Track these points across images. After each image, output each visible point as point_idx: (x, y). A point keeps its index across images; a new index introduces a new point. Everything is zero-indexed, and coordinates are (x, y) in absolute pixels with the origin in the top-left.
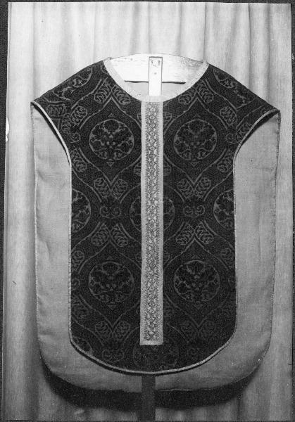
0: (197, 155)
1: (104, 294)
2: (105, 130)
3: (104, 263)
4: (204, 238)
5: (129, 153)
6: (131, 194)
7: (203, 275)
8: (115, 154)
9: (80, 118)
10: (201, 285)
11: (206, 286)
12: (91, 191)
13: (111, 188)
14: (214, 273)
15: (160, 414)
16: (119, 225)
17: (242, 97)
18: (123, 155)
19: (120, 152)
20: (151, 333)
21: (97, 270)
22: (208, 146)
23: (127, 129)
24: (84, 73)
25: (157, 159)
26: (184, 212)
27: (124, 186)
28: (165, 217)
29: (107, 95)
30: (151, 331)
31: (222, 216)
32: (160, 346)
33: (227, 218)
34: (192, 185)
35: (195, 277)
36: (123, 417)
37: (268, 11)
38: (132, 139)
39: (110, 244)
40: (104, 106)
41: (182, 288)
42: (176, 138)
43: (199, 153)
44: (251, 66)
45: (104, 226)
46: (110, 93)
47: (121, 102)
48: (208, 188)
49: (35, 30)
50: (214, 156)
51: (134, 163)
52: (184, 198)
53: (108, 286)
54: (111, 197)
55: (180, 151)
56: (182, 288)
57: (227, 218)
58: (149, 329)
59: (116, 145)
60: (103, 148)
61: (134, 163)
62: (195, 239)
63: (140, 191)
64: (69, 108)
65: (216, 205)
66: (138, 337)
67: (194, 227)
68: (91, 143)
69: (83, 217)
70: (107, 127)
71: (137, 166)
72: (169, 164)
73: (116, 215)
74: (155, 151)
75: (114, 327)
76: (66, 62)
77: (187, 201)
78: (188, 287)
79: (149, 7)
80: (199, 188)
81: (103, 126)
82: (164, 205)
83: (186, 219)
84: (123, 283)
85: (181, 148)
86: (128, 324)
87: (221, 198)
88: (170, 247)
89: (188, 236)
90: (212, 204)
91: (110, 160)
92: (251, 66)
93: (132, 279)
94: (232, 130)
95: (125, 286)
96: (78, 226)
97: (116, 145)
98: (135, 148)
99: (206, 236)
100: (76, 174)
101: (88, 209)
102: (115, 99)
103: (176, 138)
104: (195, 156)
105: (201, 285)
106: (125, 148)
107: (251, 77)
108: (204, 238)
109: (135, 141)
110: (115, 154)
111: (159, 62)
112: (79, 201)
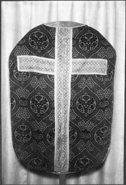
1: (36, 45)
2: (36, 99)
9: (24, 157)
13: (86, 125)
15: (72, 181)
16: (42, 78)
19: (92, 47)
22: (92, 107)
29: (37, 84)
34: (87, 85)
35: (88, 40)
36: (46, 181)
37: (115, 5)
39: (38, 150)
41: (80, 107)
44: (107, 23)
45: (35, 78)
46: (38, 83)
52: (100, 99)
54: (85, 129)
56: (80, 107)
59: (41, 43)
70: (36, 35)
73: (40, 138)
76: (26, 4)
77: (83, 131)
78: (82, 106)
84: (44, 105)
91: (38, 114)
92: (107, 23)
97: (41, 43)
108: (90, 85)
109: (49, 42)
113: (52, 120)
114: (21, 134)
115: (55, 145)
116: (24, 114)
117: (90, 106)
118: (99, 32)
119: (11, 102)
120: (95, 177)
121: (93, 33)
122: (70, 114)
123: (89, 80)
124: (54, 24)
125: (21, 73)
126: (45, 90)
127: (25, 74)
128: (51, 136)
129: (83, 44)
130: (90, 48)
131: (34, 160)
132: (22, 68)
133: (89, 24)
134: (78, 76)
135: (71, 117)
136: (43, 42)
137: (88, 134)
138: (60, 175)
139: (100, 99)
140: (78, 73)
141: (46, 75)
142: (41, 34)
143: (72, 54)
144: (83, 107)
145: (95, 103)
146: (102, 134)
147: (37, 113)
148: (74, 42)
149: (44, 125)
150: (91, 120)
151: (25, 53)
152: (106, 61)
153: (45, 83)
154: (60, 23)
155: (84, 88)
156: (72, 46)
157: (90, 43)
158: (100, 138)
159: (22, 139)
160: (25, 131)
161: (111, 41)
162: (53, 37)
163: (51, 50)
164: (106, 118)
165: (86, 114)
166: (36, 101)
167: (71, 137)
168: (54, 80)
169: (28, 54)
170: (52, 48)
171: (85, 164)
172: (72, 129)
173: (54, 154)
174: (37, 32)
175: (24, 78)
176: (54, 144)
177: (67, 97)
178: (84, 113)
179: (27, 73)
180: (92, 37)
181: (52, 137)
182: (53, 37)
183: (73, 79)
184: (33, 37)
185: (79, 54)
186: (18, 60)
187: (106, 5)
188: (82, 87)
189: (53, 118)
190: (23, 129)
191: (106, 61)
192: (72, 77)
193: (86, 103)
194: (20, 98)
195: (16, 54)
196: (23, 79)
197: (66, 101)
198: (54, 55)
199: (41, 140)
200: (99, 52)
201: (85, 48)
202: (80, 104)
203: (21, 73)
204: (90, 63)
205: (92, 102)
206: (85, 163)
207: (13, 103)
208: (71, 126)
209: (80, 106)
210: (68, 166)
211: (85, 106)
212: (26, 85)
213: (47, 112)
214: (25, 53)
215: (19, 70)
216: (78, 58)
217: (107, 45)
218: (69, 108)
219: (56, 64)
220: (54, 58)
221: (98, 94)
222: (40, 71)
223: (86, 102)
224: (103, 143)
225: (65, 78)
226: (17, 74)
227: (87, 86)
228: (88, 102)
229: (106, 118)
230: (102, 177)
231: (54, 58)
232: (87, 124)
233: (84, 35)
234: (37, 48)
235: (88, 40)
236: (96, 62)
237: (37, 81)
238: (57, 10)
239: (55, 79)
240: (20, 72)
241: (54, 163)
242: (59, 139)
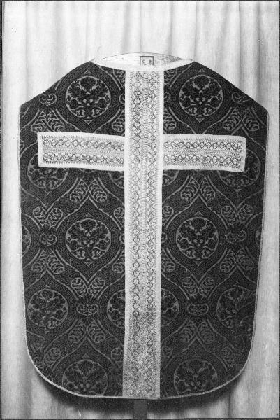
8: (93, 111)
10: (202, 241)
11: (207, 243)
21: (76, 227)
23: (103, 86)
27: (211, 283)
35: (197, 234)
49: (27, 37)
52: (227, 225)
53: (85, 242)
54: (198, 295)
59: (94, 102)
60: (190, 247)
68: (178, 242)
77: (231, 228)
97: (94, 102)
105: (202, 241)
107: (241, 75)
109: (112, 96)
110: (93, 111)
111: (150, 61)
113: (118, 272)
114: (41, 310)
115: (126, 328)
116: (55, 264)
117: (207, 243)
118: (224, 77)
119: (23, 238)
120: (218, 410)
122: (162, 260)
125: (46, 172)
126: (104, 208)
127: (55, 172)
128: (116, 306)
130: (205, 109)
131: (75, 365)
132: (49, 160)
133: (206, 60)
134: (177, 173)
135: (165, 267)
136: (97, 99)
138: (136, 402)
139: (227, 225)
140: (178, 167)
141: (105, 172)
142: (93, 82)
143: (164, 125)
145: (216, 234)
146: (232, 303)
148: (168, 95)
149: (101, 284)
150: (209, 273)
151: (55, 127)
152: (241, 141)
153: (105, 191)
156: (163, 107)
157: (204, 99)
158: (228, 313)
159: (45, 322)
160: (51, 304)
162: (120, 86)
163: (116, 115)
164: (240, 269)
167: (165, 312)
168: (123, 182)
169: (62, 128)
170: (118, 112)
172: (167, 294)
173: (122, 349)
175: (50, 182)
176: (123, 325)
177: (154, 220)
179: (60, 170)
181: (118, 310)
182: (120, 86)
183: (167, 180)
184: (75, 92)
185: (179, 124)
186: (40, 141)
188: (189, 198)
189: (122, 267)
190: (48, 299)
191: (241, 141)
192: (163, 176)
193: (198, 236)
194: (40, 229)
195: (35, 128)
196: (49, 185)
197: (137, 112)
198: (124, 127)
200: (224, 120)
203: (46, 172)
204: (206, 145)
205: (210, 232)
206: (195, 370)
207: (25, 242)
208: (164, 288)
210: (158, 378)
212: (57, 198)
213: (106, 255)
214: (55, 127)
215: (41, 163)
216: (178, 133)
217: (244, 103)
218: (160, 245)
219: (127, 148)
220: (121, 133)
222: (90, 163)
223: (198, 234)
224: (234, 324)
225: (148, 178)
226: (37, 173)
228: (203, 233)
229: (240, 269)
230: (230, 408)
231: (121, 133)
233: (191, 81)
235: (197, 234)
236: (219, 143)
239: (125, 181)
240: (44, 169)
241: (122, 368)
242: (136, 316)
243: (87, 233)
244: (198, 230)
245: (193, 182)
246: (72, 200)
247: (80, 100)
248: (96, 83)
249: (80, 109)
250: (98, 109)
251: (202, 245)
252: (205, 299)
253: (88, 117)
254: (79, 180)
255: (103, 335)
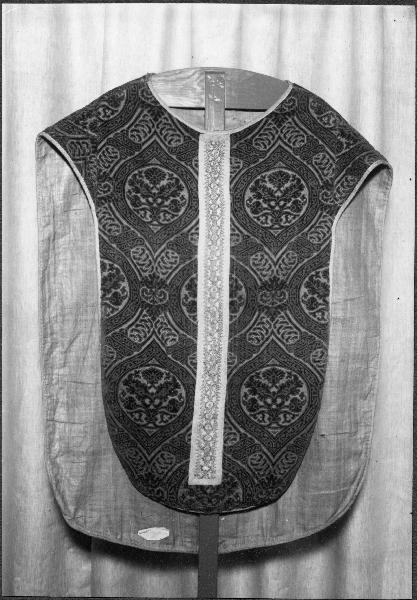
0: (281, 220)
3: (264, 370)
4: (286, 336)
5: (181, 213)
6: (183, 270)
7: (283, 387)
12: (246, 271)
13: (275, 265)
14: (177, 386)
16: (166, 316)
17: (343, 140)
18: (173, 216)
19: (289, 213)
20: (205, 468)
22: (297, 207)
24: (111, 98)
25: (222, 222)
26: (259, 298)
28: (232, 304)
30: (206, 466)
31: (312, 304)
32: (218, 487)
33: (320, 307)
34: (273, 261)
35: (150, 391)
38: (185, 193)
40: (143, 148)
41: (253, 403)
42: (249, 194)
43: (283, 217)
44: (354, 74)
45: (145, 315)
47: (294, 144)
48: (175, 266)
50: (304, 222)
51: (189, 227)
55: (254, 212)
57: (320, 307)
58: (202, 463)
59: (163, 202)
61: (189, 227)
62: (154, 337)
63: (196, 266)
64: (96, 147)
65: (304, 290)
66: (186, 473)
67: (273, 319)
68: (248, 204)
69: (117, 299)
71: (193, 231)
72: (238, 229)
74: (219, 211)
75: (152, 459)
78: (261, 403)
79: (192, 17)
80: (161, 264)
81: (267, 179)
82: (231, 286)
83: (261, 309)
85: (256, 208)
86: (172, 456)
87: (311, 278)
88: (238, 346)
89: (264, 332)
90: (298, 289)
91: (277, 226)
92: (354, 74)
93: (182, 391)
94: (328, 185)
95: (173, 402)
96: (109, 310)
97: (161, 403)
98: (190, 207)
99: (290, 333)
100: (105, 238)
101: (124, 288)
102: (285, 143)
103: (249, 194)
104: (277, 220)
106: (176, 206)
108: (286, 336)
112: (110, 275)
121: (293, 170)
123: (281, 320)
124: (182, 75)
129: (258, 204)
137: (283, 290)
144: (261, 407)
147: (150, 220)
154: (202, 74)
155: (273, 149)
157: (279, 401)
161: (369, 132)
165: (275, 428)
166: (147, 187)
171: (279, 189)
174: (148, 368)
178: (268, 423)
180: (287, 185)
187: (354, 20)
193: (274, 393)
199: (164, 307)
201: (267, 218)
202: (255, 394)
206: (274, 383)
209: (254, 401)
211: (269, 401)
221: (315, 362)
223: (274, 389)
227: (283, 145)
230: (338, 563)
232: (280, 261)
234: (151, 216)
237: (151, 125)
238: (192, 32)
243: (150, 388)
244: (279, 189)
245: (271, 127)
246: (132, 338)
247: (139, 398)
248: (167, 177)
249: (143, 209)
250: (167, 414)
251: (282, 207)
252: (283, 283)
253: (150, 425)
254: (142, 112)
255: (175, 335)
